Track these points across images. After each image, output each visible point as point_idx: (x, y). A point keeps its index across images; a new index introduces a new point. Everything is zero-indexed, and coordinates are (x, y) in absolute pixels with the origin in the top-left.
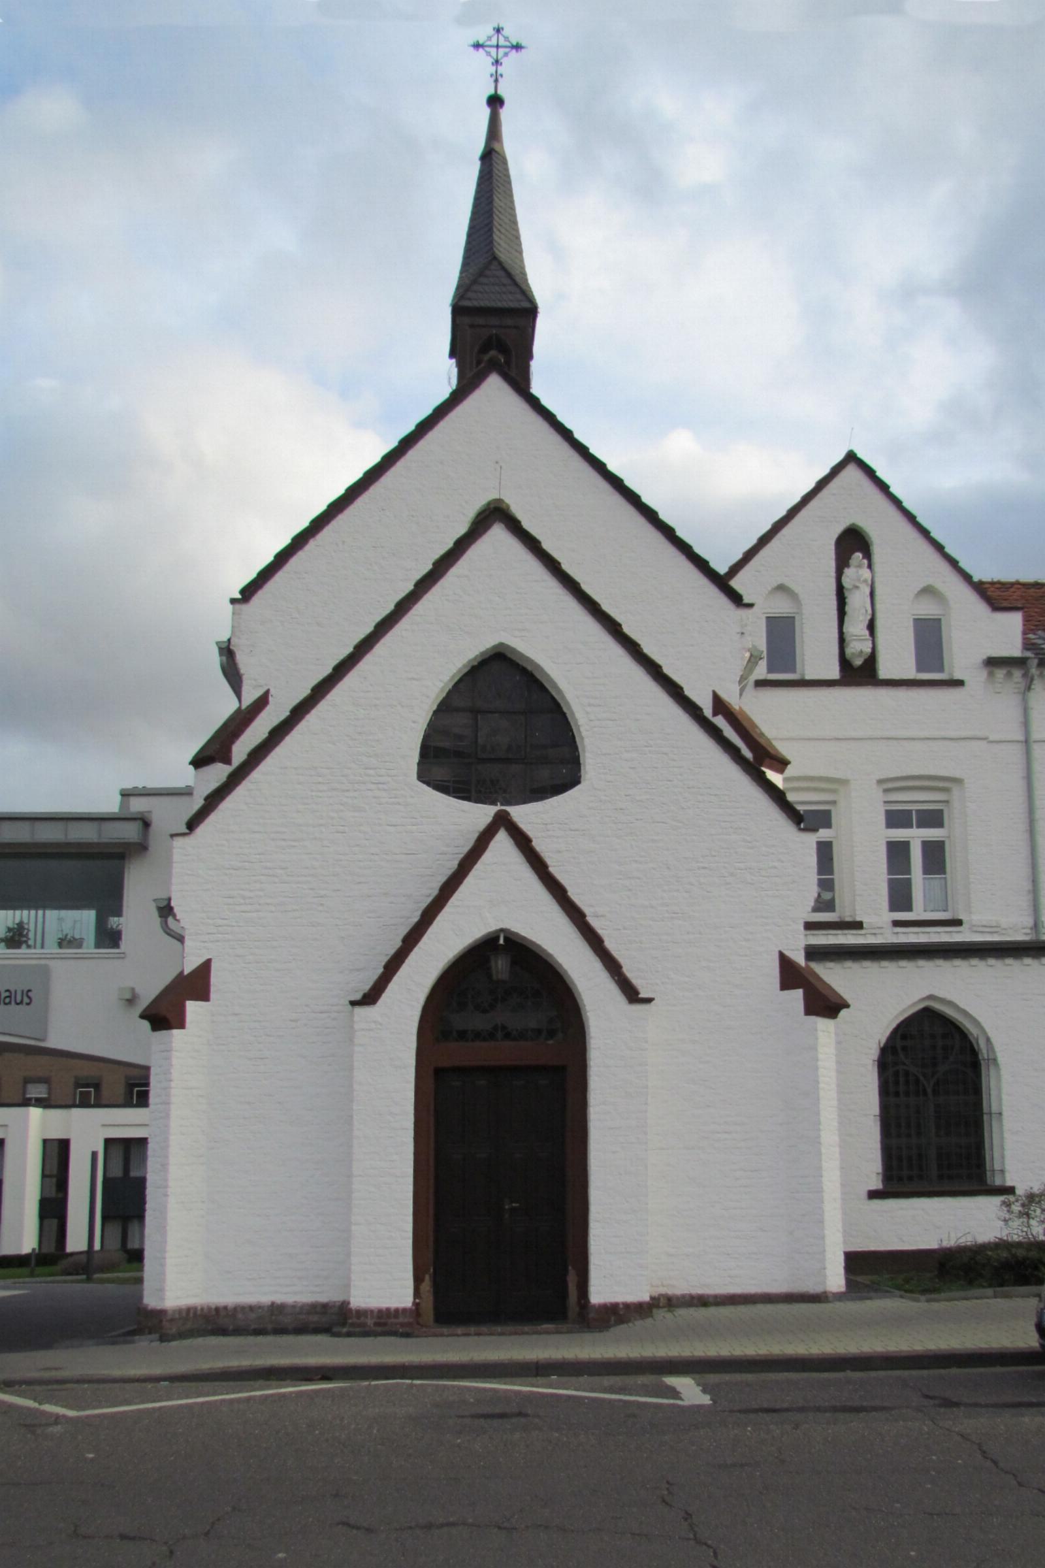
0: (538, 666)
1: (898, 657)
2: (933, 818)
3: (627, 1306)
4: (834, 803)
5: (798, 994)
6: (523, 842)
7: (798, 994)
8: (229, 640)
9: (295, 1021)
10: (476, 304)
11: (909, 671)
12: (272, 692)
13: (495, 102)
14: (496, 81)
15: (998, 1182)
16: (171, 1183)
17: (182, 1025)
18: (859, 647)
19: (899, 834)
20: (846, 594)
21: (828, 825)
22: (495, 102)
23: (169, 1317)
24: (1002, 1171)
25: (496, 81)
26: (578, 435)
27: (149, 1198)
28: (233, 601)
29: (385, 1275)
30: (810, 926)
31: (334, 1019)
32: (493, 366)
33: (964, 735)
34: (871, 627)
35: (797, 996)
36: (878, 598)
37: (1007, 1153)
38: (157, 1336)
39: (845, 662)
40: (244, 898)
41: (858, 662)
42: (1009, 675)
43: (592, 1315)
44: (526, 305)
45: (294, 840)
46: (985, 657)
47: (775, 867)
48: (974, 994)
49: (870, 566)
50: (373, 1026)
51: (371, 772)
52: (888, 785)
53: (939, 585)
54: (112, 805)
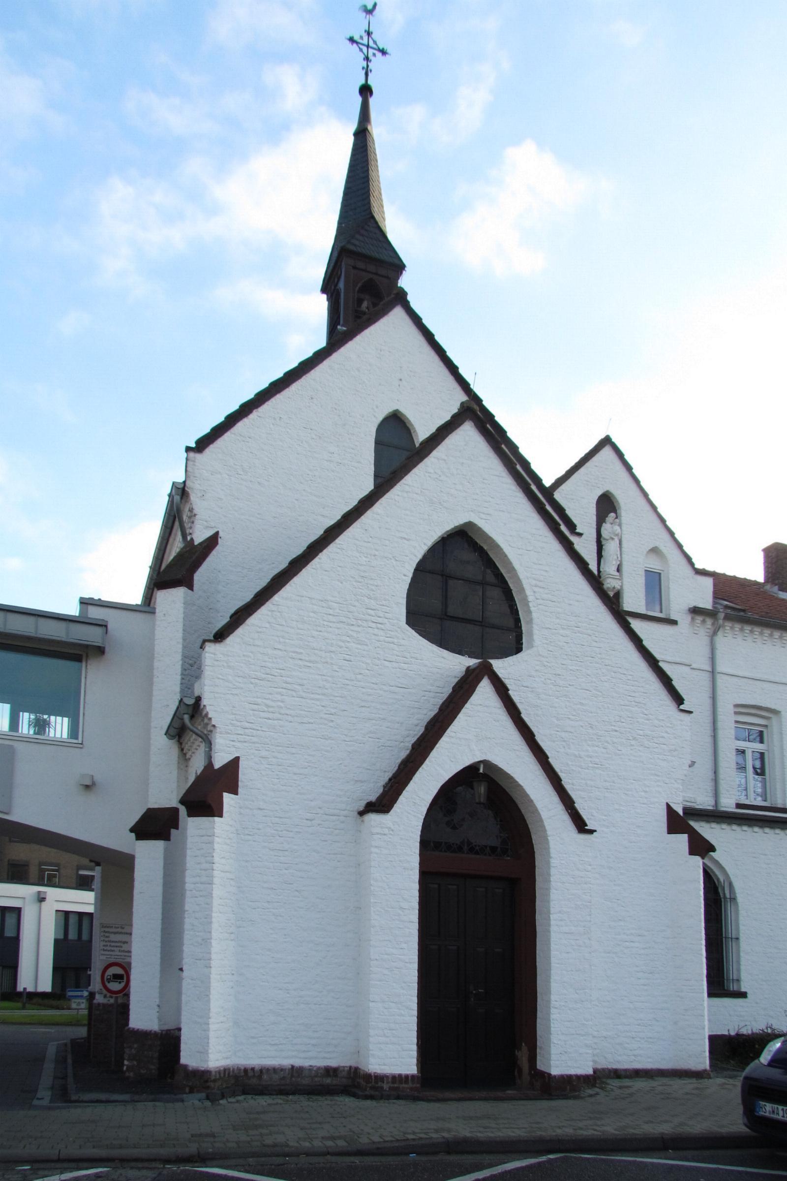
0: (497, 547)
3: (578, 1077)
6: (501, 690)
8: (184, 482)
9: (311, 820)
12: (221, 534)
13: (366, 91)
14: (367, 75)
15: (733, 987)
16: (213, 956)
17: (220, 815)
20: (603, 542)
22: (366, 91)
23: (213, 1078)
24: (738, 980)
25: (367, 75)
28: (188, 449)
29: (393, 1046)
31: (343, 822)
35: (683, 839)
37: (742, 968)
38: (203, 1095)
40: (267, 706)
45: (310, 661)
46: (687, 608)
47: (663, 737)
50: (386, 831)
51: (372, 612)
53: (662, 548)
54: (73, 610)
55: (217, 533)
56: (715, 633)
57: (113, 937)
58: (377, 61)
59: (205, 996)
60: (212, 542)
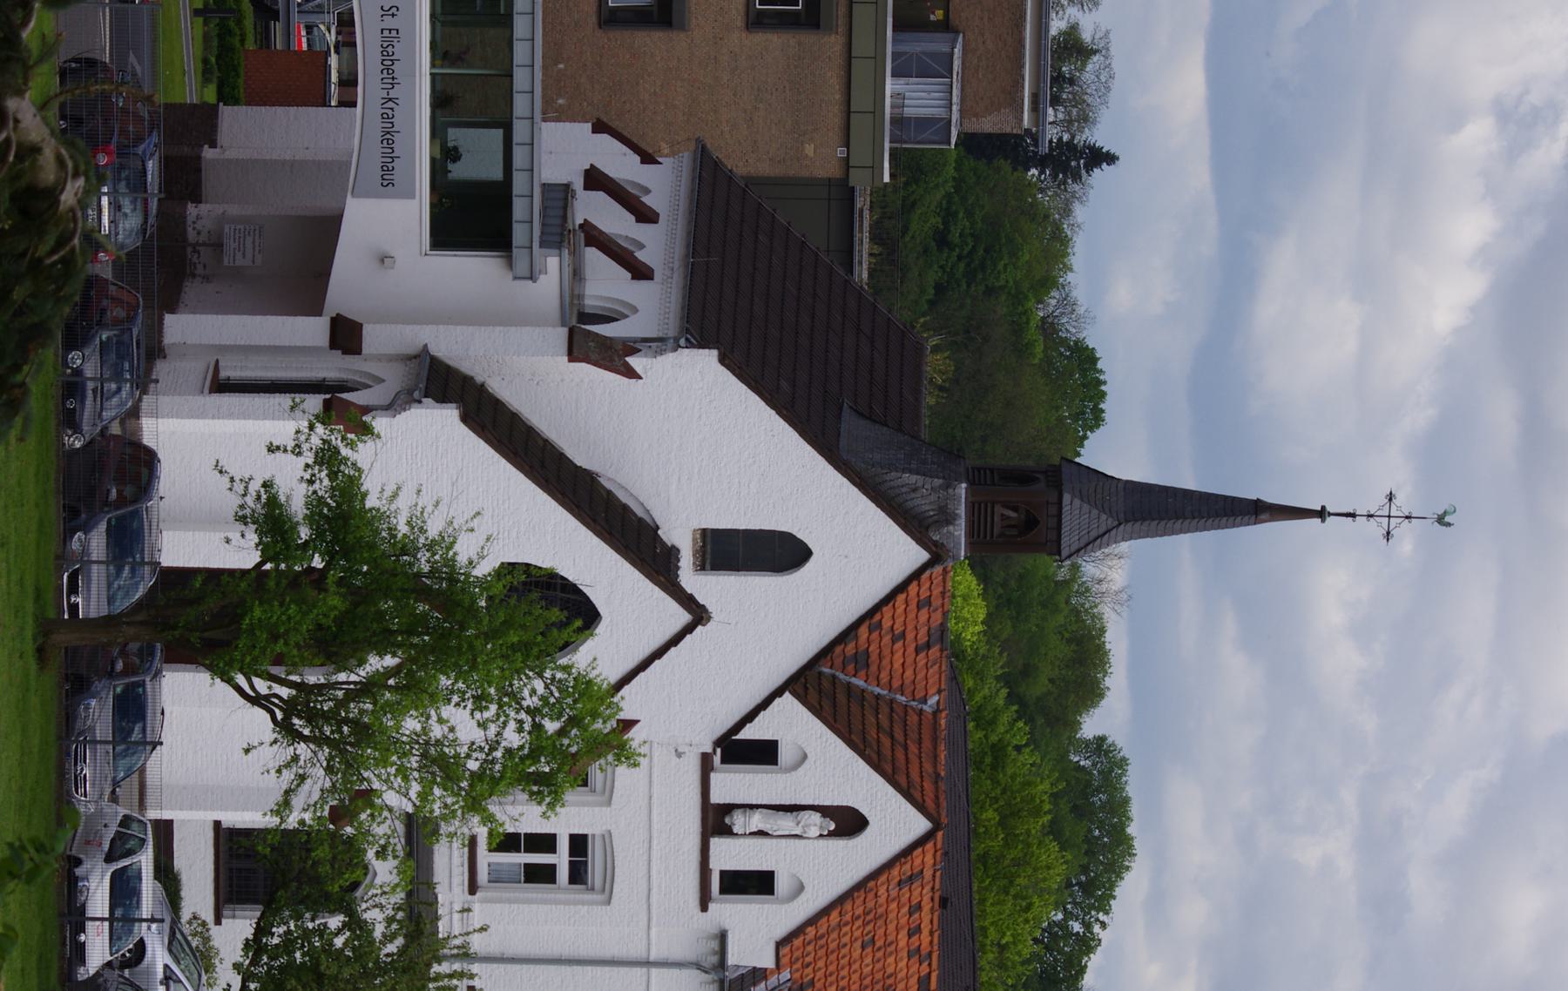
1: (729, 855)
2: (578, 874)
10: (1066, 509)
15: (225, 913)
18: (738, 821)
19: (563, 845)
24: (234, 917)
34: (761, 833)
36: (792, 841)
39: (729, 809)
42: (715, 953)
52: (607, 838)
53: (803, 897)
55: (640, 378)
56: (698, 966)
57: (249, 240)
58: (1375, 529)
59: (193, 415)
60: (631, 373)
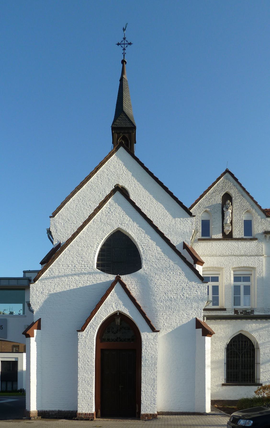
4: (251, 274)
5: (200, 330)
6: (124, 286)
7: (200, 330)
11: (242, 235)
14: (124, 55)
18: (228, 229)
19: (238, 283)
21: (218, 281)
22: (123, 62)
25: (124, 55)
26: (145, 165)
27: (143, 378)
30: (205, 310)
32: (121, 145)
33: (249, 255)
41: (227, 233)
43: (141, 417)
44: (128, 125)
48: (254, 330)
49: (232, 204)
54: (21, 275)
